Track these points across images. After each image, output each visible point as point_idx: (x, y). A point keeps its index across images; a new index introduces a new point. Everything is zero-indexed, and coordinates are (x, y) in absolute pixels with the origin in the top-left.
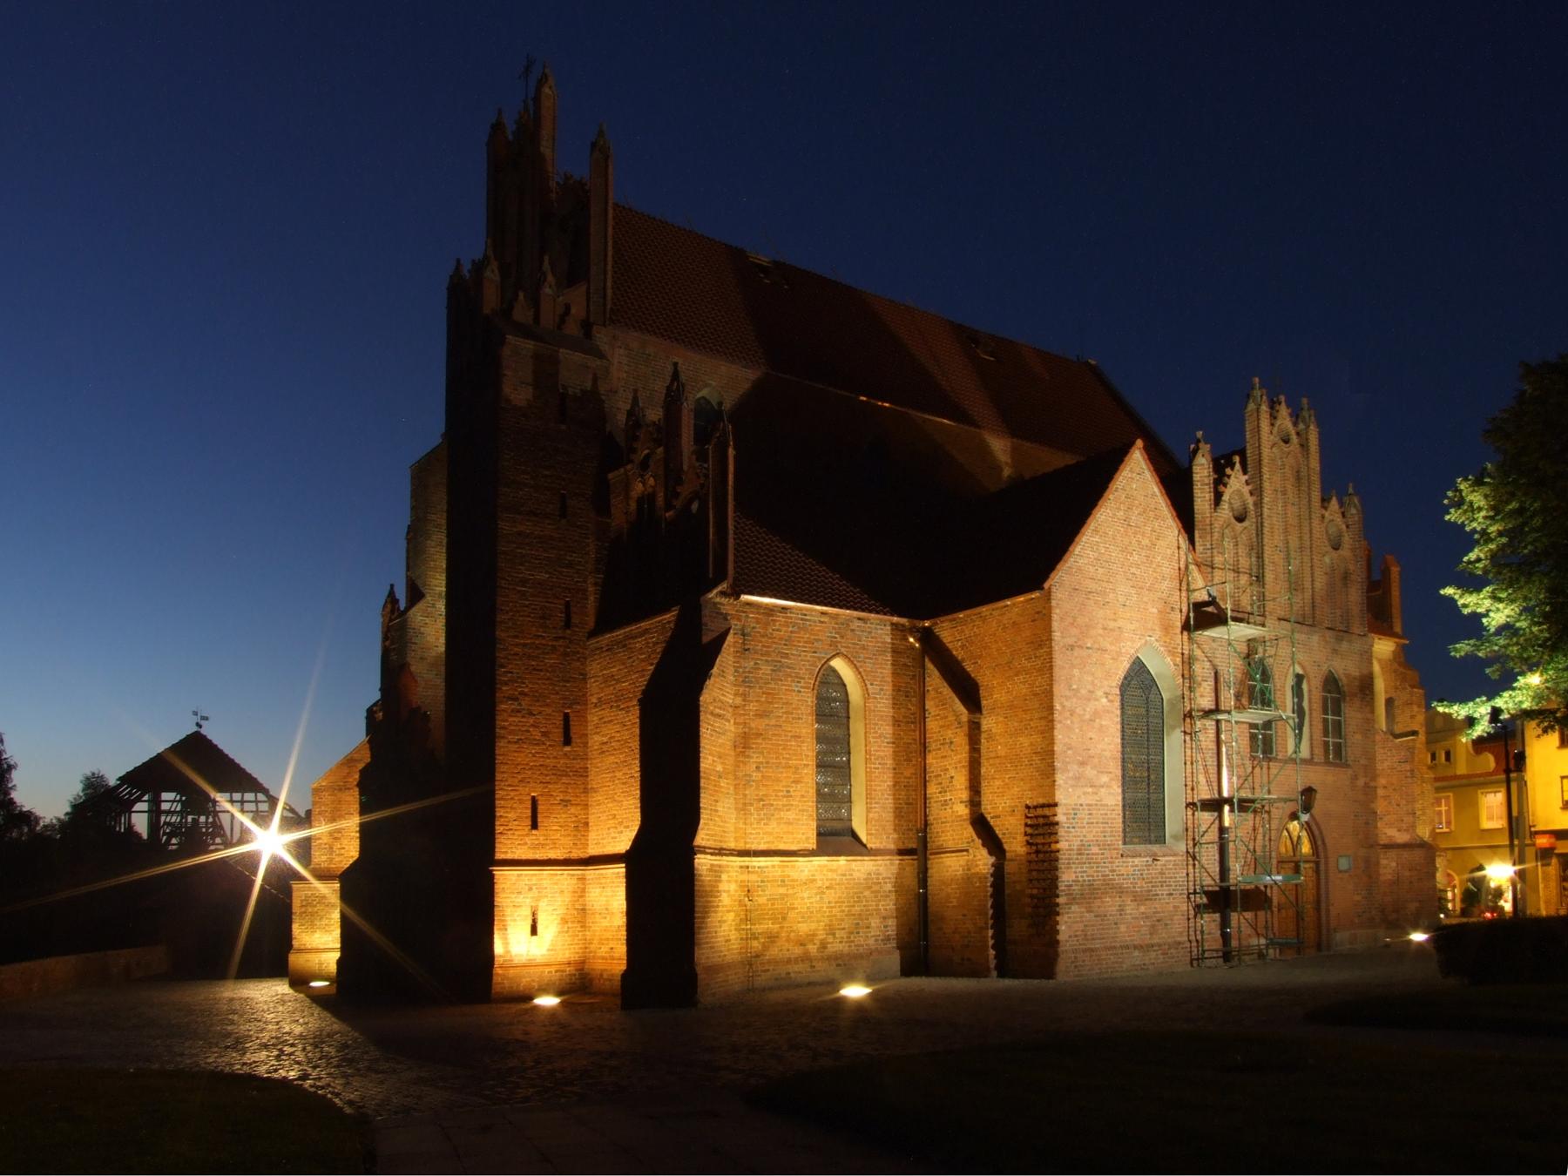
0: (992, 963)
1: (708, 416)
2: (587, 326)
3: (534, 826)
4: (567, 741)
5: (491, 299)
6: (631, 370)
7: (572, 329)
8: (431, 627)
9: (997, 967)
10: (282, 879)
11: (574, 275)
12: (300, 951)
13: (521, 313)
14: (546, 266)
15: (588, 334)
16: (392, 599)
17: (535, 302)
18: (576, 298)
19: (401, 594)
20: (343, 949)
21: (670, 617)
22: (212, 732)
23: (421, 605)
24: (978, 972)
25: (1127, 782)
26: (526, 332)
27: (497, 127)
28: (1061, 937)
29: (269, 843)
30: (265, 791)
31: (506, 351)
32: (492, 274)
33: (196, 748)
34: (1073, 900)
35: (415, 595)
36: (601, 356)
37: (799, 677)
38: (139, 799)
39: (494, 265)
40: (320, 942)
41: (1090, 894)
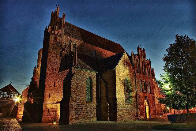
0: (109, 119)
1: (75, 46)
2: (61, 34)
3: (49, 98)
4: (54, 86)
5: (49, 30)
6: (65, 40)
7: (59, 34)
8: (39, 71)
9: (109, 120)
10: (18, 104)
11: (60, 28)
12: (19, 114)
13: (53, 32)
14: (56, 27)
15: (61, 35)
16: (35, 67)
17: (55, 31)
18: (60, 31)
19: (36, 67)
20: (23, 114)
21: (68, 70)
22: (12, 85)
23: (38, 68)
24: (107, 120)
25: (45, 72)
26: (53, 34)
27: (53, 12)
28: (118, 116)
29: (17, 99)
30: (18, 92)
31: (51, 36)
32: (50, 27)
33: (10, 85)
34: (119, 111)
35: (38, 67)
36: (62, 38)
37: (19, 94)
38: (2, 93)
39: (50, 26)
40: (21, 113)
41: (121, 110)
